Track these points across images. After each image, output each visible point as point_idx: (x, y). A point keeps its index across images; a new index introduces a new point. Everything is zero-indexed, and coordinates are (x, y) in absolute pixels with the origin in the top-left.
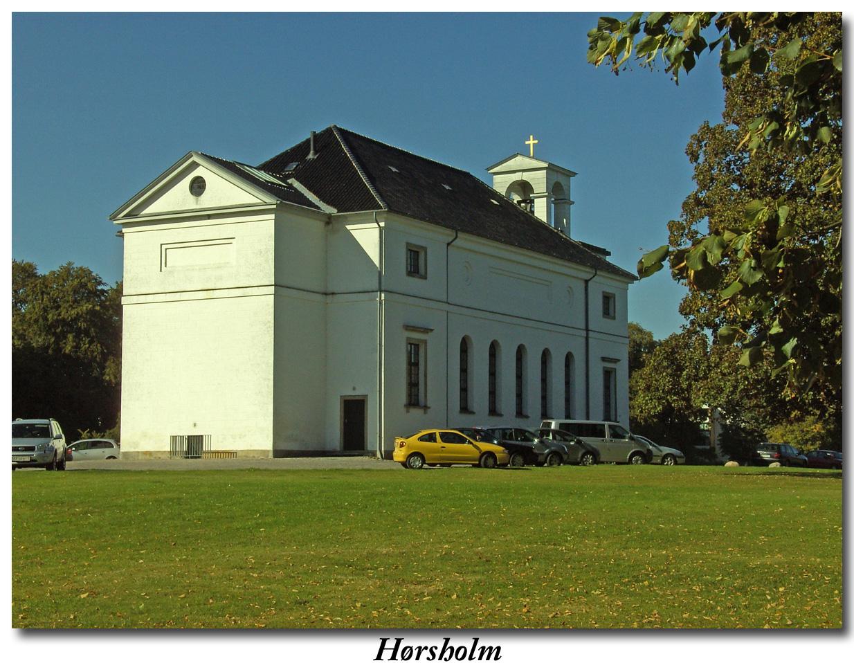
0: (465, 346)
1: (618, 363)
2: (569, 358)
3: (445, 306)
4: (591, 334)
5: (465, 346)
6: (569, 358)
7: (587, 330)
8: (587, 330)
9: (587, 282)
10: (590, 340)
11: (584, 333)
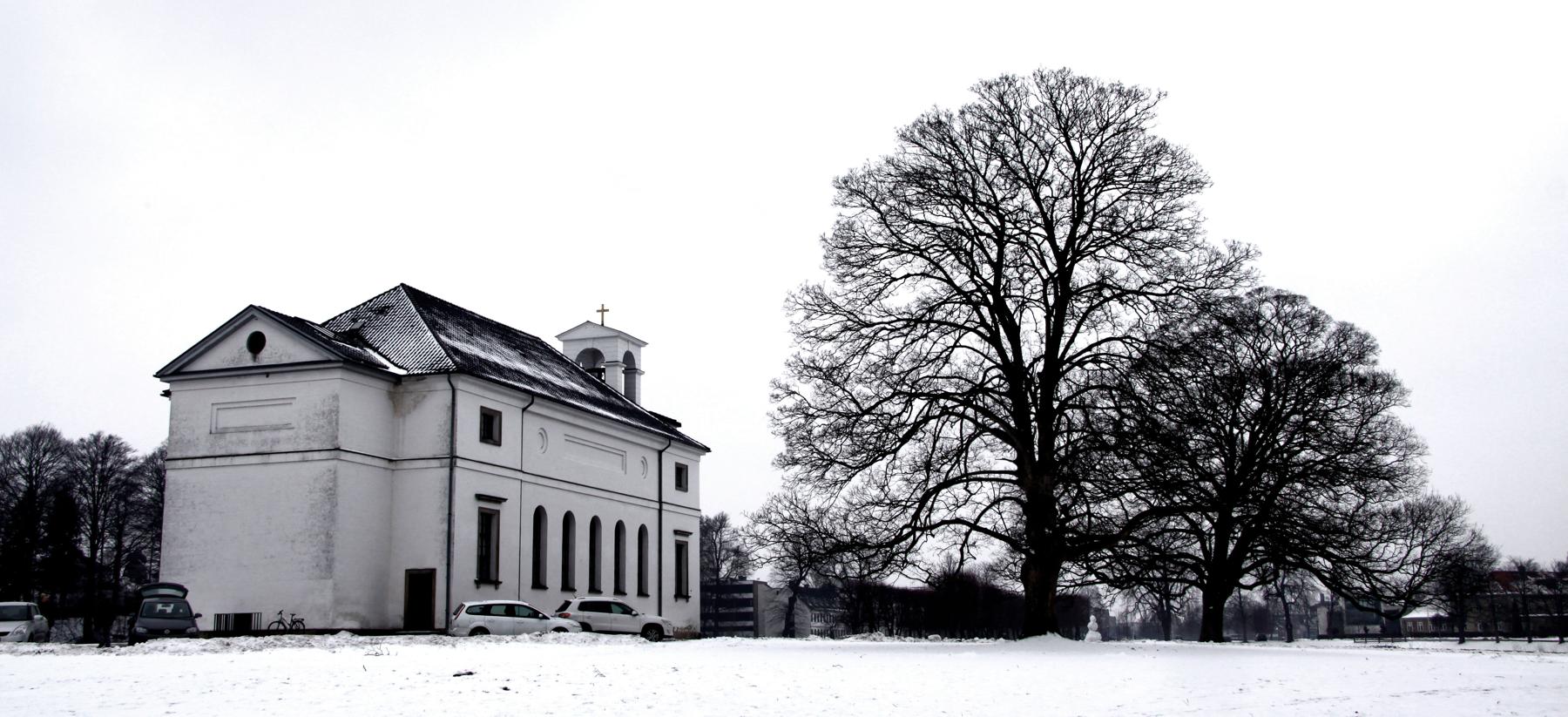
0: (540, 514)
1: (504, 503)
2: (643, 531)
3: (520, 476)
4: (664, 507)
5: (540, 514)
6: (643, 531)
7: (660, 502)
8: (660, 502)
9: (660, 453)
10: (663, 513)
11: (657, 506)
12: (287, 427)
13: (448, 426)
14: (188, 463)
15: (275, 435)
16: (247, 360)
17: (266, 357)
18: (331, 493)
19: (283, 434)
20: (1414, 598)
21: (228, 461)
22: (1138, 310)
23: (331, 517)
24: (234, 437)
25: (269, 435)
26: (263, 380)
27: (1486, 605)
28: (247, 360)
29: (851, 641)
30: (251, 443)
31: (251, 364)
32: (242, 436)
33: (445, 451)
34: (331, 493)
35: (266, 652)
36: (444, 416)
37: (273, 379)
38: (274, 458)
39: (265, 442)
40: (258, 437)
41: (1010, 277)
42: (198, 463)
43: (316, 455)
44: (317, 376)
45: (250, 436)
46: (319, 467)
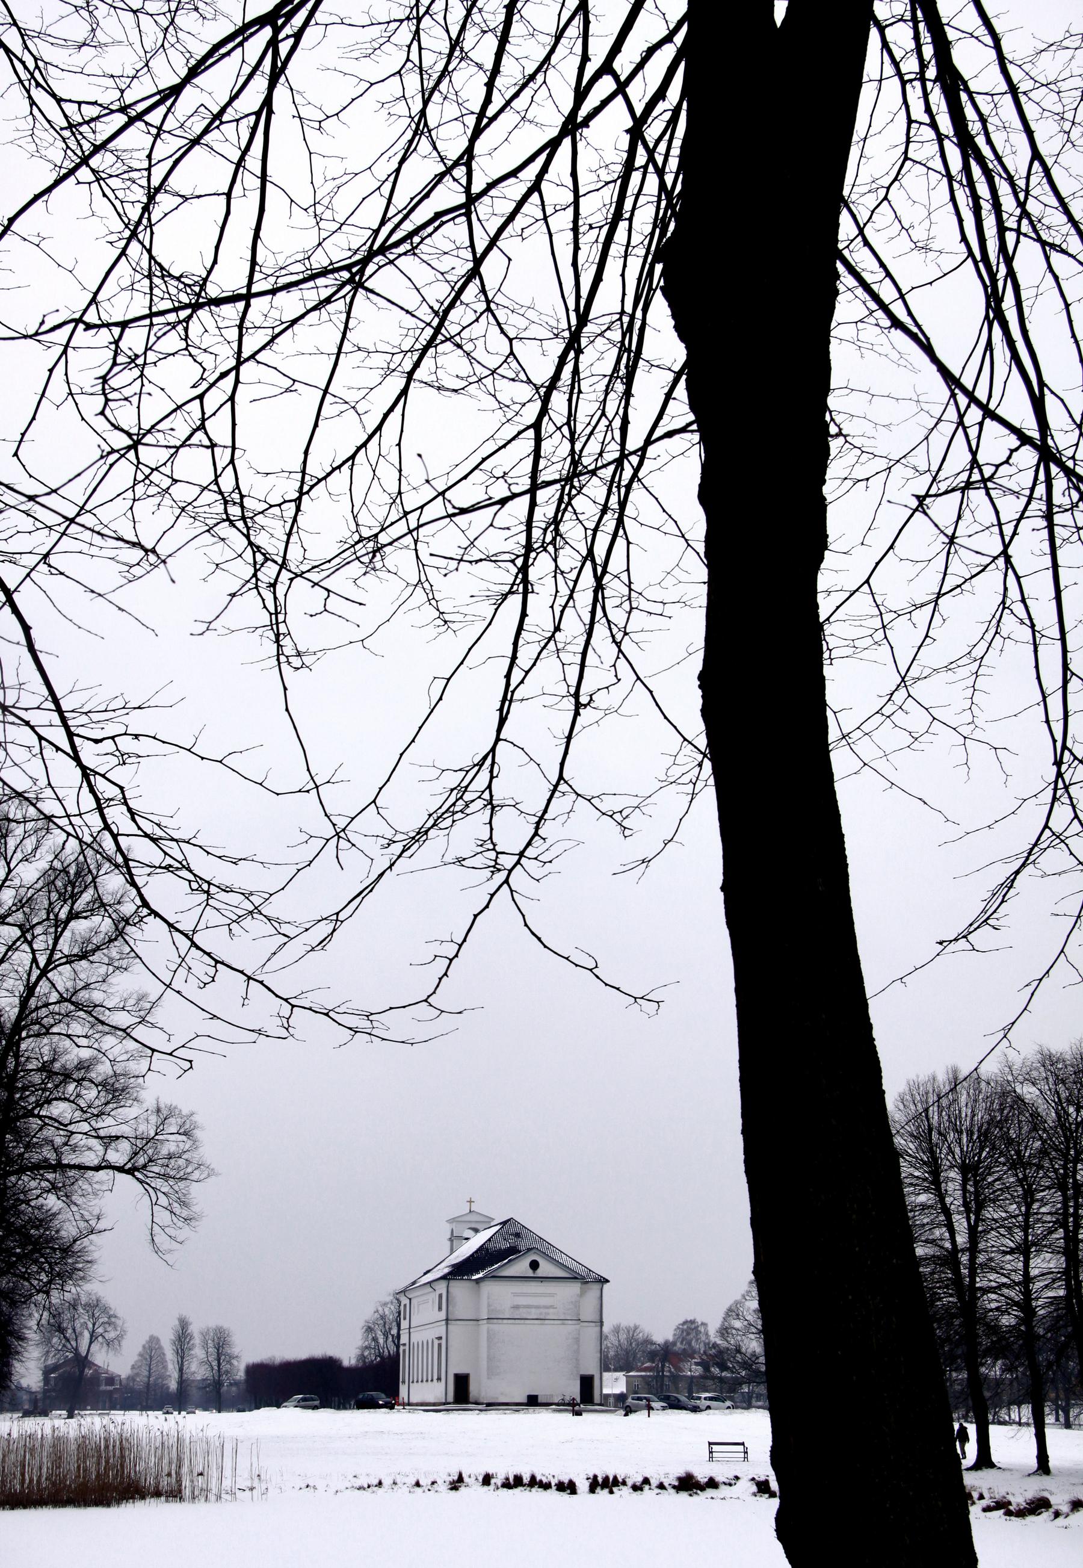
12: (552, 1307)
13: (599, 1306)
14: (500, 1321)
15: (546, 1310)
16: (530, 1273)
17: (540, 1272)
18: (577, 1340)
19: (551, 1310)
20: (743, 1373)
21: (522, 1321)
22: (184, 50)
23: (577, 1351)
24: (525, 1310)
25: (544, 1311)
26: (539, 1284)
27: (22, 1150)
28: (530, 1273)
29: (361, 1411)
30: (534, 1313)
31: (532, 1275)
32: (529, 1310)
33: (597, 1318)
34: (577, 1340)
35: (735, 1416)
36: (596, 1302)
37: (543, 1284)
38: (547, 1322)
39: (541, 1314)
40: (538, 1311)
41: (228, 498)
42: (505, 1321)
43: (570, 1322)
44: (568, 1284)
45: (533, 1310)
46: (571, 1328)
